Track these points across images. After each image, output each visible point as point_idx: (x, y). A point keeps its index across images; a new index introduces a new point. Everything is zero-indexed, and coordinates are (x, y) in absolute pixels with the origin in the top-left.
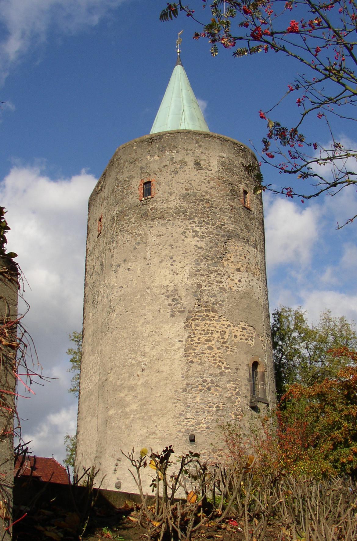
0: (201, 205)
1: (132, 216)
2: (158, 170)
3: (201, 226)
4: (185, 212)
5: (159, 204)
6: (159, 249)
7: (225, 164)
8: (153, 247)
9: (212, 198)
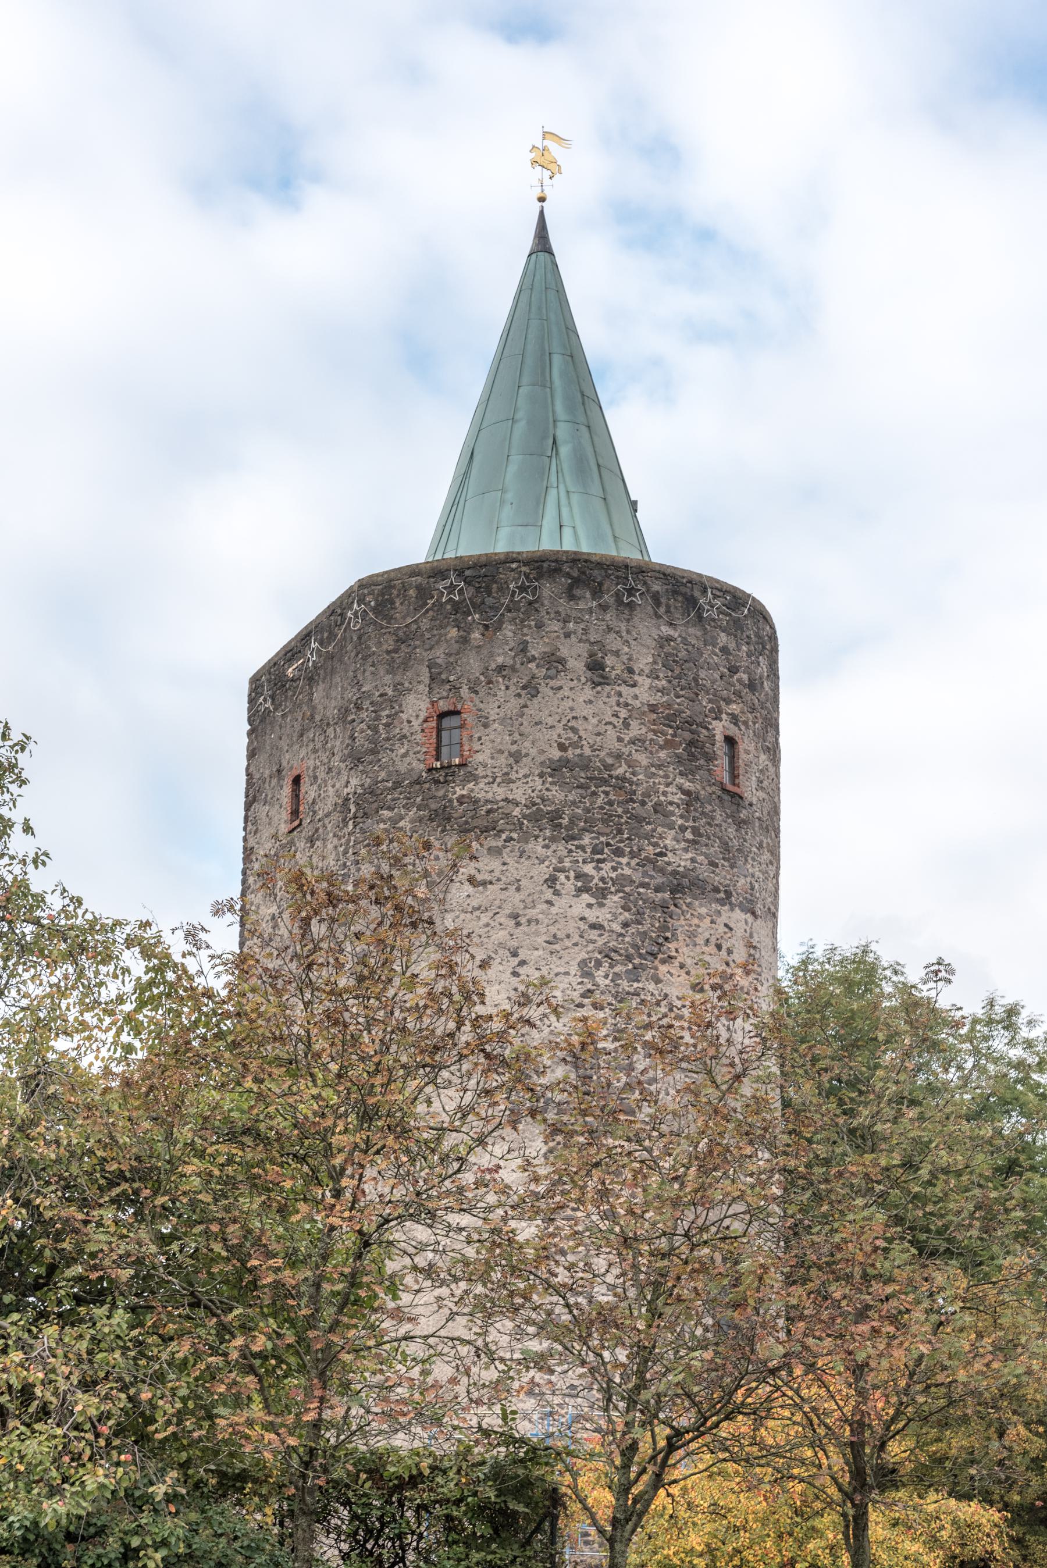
0: (603, 796)
1: (403, 811)
2: (482, 678)
3: (599, 861)
4: (556, 815)
5: (481, 785)
6: (481, 923)
7: (674, 661)
8: (462, 916)
9: (634, 774)
